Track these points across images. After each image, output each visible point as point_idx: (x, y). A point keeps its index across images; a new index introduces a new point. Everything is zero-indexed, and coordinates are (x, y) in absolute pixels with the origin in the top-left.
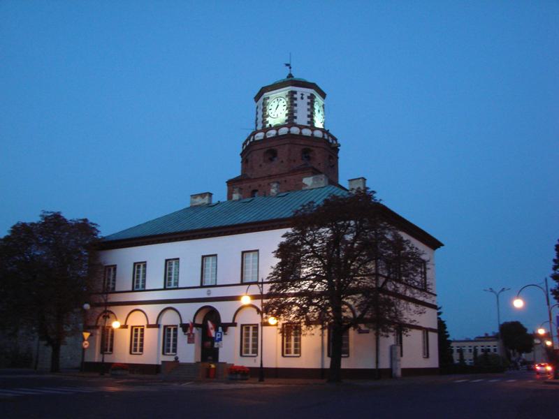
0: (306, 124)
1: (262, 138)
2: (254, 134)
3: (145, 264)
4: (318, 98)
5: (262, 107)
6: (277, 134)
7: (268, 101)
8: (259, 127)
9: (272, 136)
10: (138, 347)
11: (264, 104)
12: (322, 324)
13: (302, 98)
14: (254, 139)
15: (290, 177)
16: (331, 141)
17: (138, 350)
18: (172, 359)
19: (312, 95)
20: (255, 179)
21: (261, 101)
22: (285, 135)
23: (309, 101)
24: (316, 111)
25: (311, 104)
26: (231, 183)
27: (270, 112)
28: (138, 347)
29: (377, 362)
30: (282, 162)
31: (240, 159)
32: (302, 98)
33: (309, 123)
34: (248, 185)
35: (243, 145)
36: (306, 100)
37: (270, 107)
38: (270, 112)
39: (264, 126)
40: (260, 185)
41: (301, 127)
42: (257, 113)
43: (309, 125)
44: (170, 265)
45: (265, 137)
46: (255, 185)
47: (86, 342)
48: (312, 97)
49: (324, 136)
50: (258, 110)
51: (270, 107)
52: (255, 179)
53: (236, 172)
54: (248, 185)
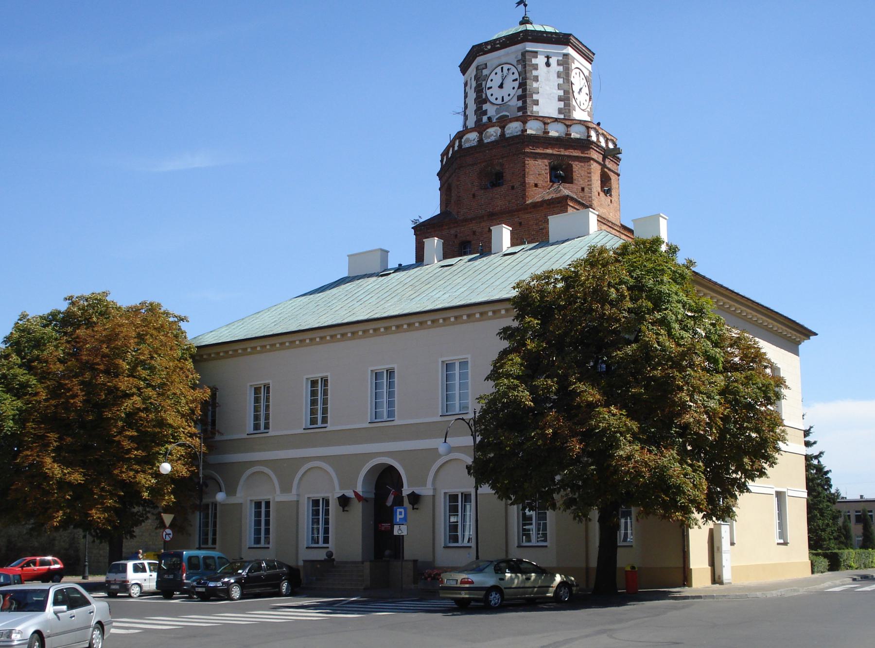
0: (555, 115)
1: (475, 143)
2: (460, 136)
3: (267, 388)
4: (578, 61)
5: (474, 84)
6: (503, 134)
7: (485, 72)
8: (471, 123)
9: (493, 138)
10: (320, 416)
11: (477, 78)
12: (523, 502)
13: (548, 64)
14: (460, 146)
15: (527, 216)
16: (603, 144)
17: (210, 541)
18: (321, 555)
19: (566, 56)
20: (466, 221)
21: (472, 71)
22: (517, 136)
23: (561, 68)
24: (576, 88)
25: (565, 75)
27: (489, 92)
28: (320, 416)
29: (507, 552)
30: (513, 188)
31: (438, 184)
32: (548, 64)
33: (560, 111)
34: (453, 232)
35: (442, 155)
36: (555, 67)
37: (489, 84)
38: (489, 92)
39: (478, 121)
40: (474, 233)
41: (545, 121)
42: (466, 97)
43: (562, 116)
44: (318, 389)
45: (480, 140)
47: (168, 531)
48: (565, 62)
50: (468, 88)
51: (489, 84)
52: (466, 221)
53: (430, 206)
54: (453, 232)
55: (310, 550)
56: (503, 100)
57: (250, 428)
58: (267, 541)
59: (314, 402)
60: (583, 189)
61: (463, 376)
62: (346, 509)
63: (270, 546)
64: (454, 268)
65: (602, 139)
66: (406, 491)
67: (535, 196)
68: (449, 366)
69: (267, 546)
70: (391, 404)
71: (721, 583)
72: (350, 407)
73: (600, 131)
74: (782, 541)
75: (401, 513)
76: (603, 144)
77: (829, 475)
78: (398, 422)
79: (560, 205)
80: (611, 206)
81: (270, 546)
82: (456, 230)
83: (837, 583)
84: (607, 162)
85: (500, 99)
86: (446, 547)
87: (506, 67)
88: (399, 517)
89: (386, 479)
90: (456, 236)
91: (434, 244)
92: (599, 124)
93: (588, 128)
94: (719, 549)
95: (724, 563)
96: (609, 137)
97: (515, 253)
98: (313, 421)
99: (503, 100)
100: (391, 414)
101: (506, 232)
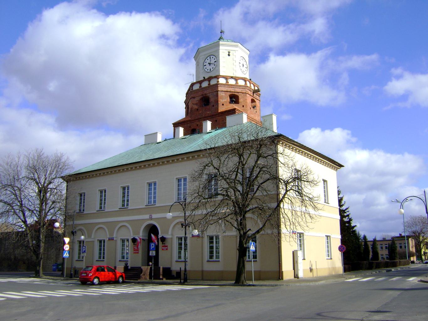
2: (192, 85)
15: (219, 118)
26: (176, 125)
46: (193, 126)
49: (246, 84)
54: (189, 125)
55: (178, 263)
56: (210, 70)
57: (98, 208)
58: (217, 257)
59: (124, 197)
60: (243, 106)
61: (185, 185)
62: (164, 243)
63: (220, 259)
64: (186, 139)
65: (252, 85)
66: (160, 236)
67: (221, 109)
68: (179, 180)
69: (103, 260)
70: (155, 197)
71: (298, 278)
72: (138, 199)
73: (251, 82)
74: (329, 258)
75: (153, 246)
76: (253, 88)
77: (355, 228)
78: (157, 205)
79: (232, 112)
80: (256, 113)
81: (220, 259)
82: (191, 125)
83: (352, 279)
84: (255, 95)
85: (209, 70)
86: (208, 261)
87: (211, 57)
88: (152, 247)
89: (153, 229)
90: (190, 127)
91: (181, 130)
92: (250, 80)
93: (245, 81)
94: (297, 262)
95: (299, 268)
96: (256, 85)
97: (212, 132)
98: (123, 205)
99: (210, 70)
100: (155, 202)
101: (209, 124)
